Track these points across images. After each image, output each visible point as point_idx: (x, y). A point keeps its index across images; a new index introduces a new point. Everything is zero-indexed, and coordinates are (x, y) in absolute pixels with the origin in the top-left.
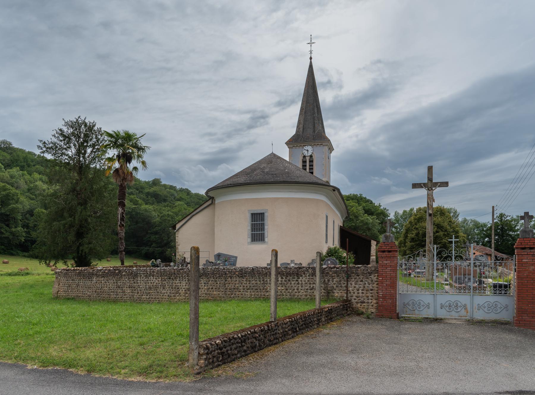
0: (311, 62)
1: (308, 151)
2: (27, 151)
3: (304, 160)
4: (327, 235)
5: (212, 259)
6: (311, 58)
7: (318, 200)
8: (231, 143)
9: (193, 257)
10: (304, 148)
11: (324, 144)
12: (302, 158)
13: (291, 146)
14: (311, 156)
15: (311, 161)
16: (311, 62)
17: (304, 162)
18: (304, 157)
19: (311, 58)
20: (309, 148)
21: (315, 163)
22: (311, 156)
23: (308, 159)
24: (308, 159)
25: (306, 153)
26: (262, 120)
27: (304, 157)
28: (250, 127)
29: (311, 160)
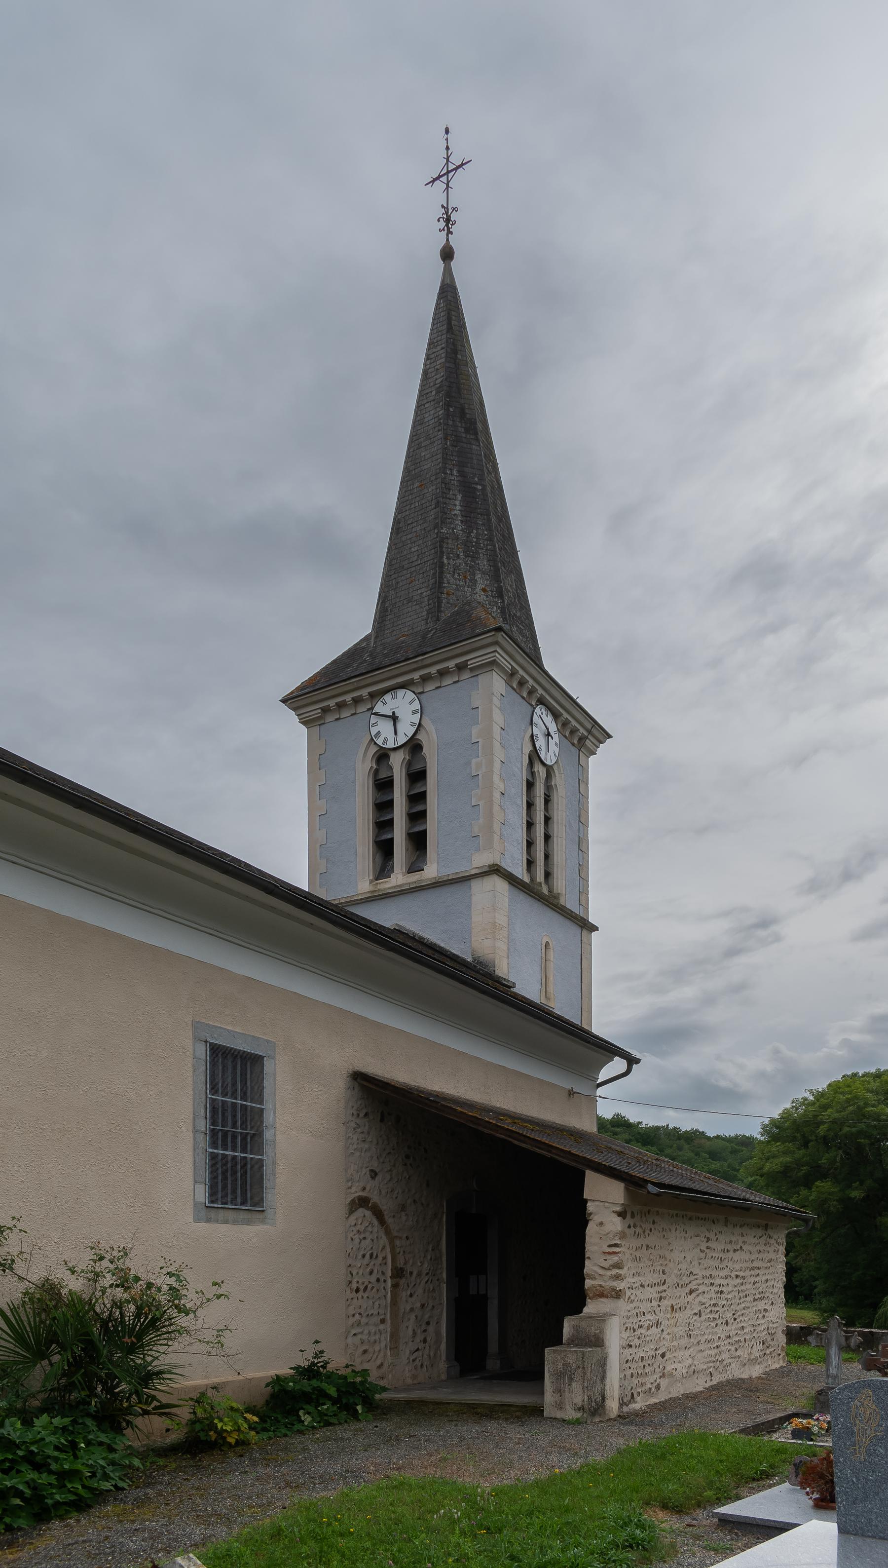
0: (448, 273)
1: (394, 718)
2: (683, 1130)
3: (383, 775)
5: (133, 1272)
6: (447, 254)
8: (685, 994)
10: (379, 708)
11: (473, 658)
13: (314, 711)
14: (414, 746)
16: (448, 273)
18: (383, 756)
19: (447, 254)
20: (403, 704)
21: (431, 785)
22: (414, 746)
24: (397, 761)
26: (761, 933)
27: (383, 756)
28: (732, 952)
29: (417, 767)
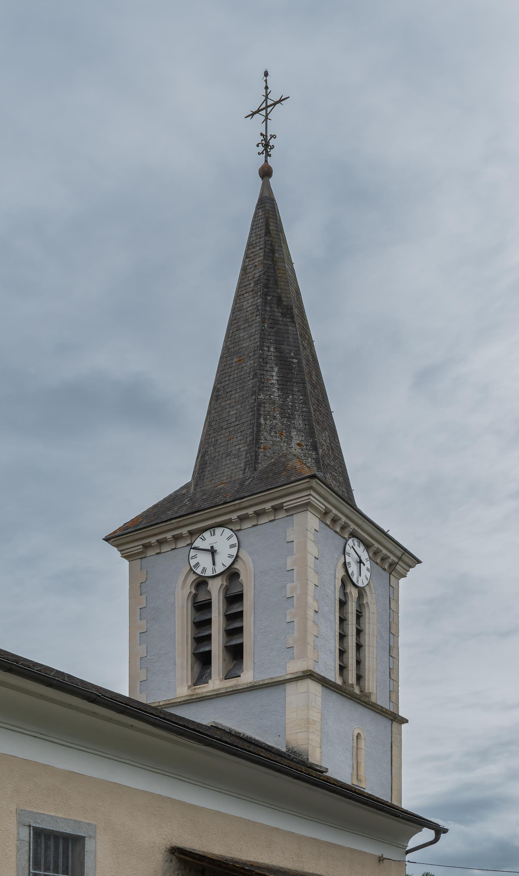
0: (266, 188)
1: (213, 552)
3: (202, 598)
4: (392, 755)
6: (266, 173)
7: (352, 851)
9: (314, 773)
10: (198, 543)
11: (289, 501)
12: (189, 589)
13: (136, 547)
14: (232, 574)
15: (234, 598)
16: (266, 188)
17: (202, 607)
18: (201, 583)
19: (266, 173)
20: (222, 541)
22: (232, 574)
23: (216, 590)
24: (216, 590)
25: (204, 564)
27: (201, 583)
29: (235, 591)
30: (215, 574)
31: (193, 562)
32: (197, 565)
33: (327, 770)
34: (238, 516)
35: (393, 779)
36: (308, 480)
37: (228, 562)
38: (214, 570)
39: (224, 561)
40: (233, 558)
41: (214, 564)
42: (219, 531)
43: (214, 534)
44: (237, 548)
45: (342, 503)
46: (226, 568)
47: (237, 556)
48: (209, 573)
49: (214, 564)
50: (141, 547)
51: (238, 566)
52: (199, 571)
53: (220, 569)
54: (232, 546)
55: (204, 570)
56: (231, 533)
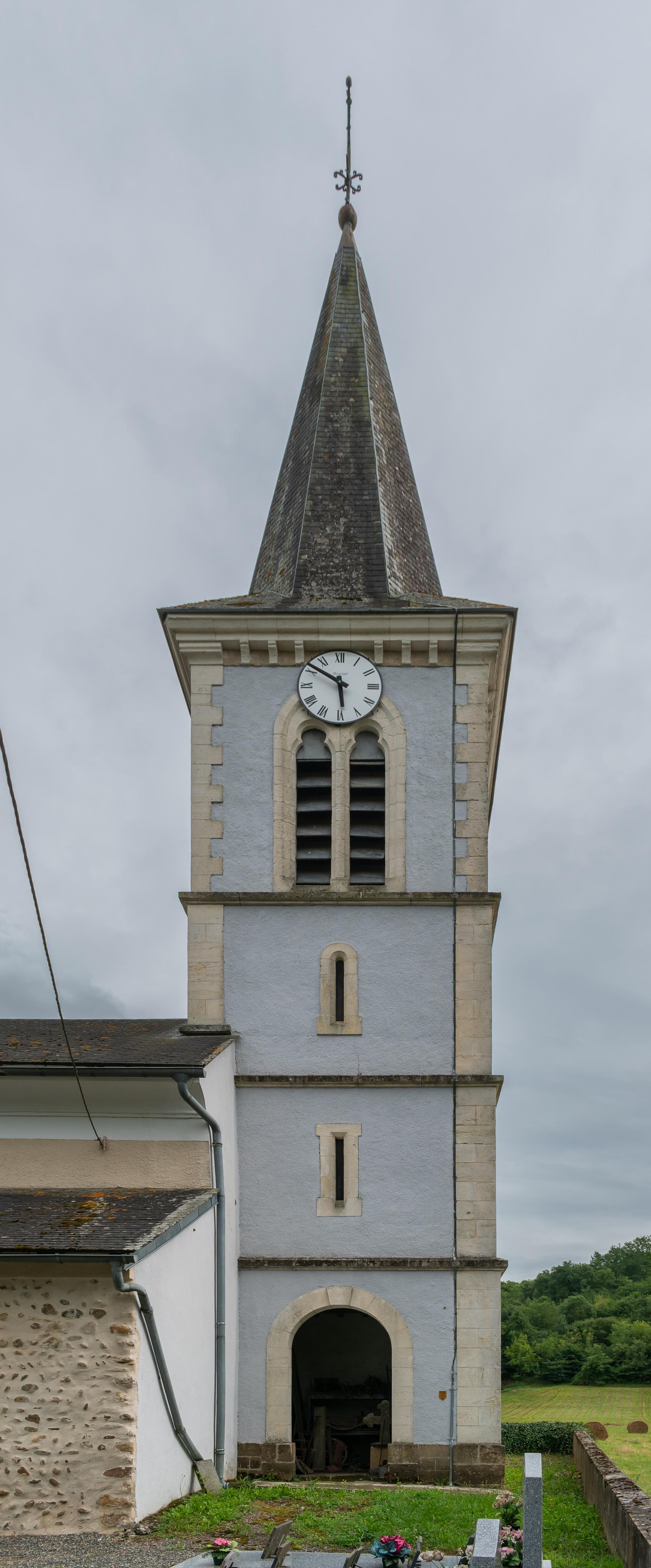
14: (366, 731)
17: (312, 770)
18: (315, 730)
22: (366, 731)
25: (324, 700)
27: (315, 730)
30: (341, 721)
31: (305, 694)
32: (312, 699)
33: (597, 1255)
34: (384, 642)
35: (458, 1002)
36: (504, 616)
37: (365, 710)
38: (340, 715)
39: (357, 705)
40: (373, 706)
41: (342, 704)
42: (350, 658)
43: (343, 661)
44: (380, 691)
45: (247, 619)
46: (360, 717)
47: (379, 705)
48: (331, 717)
49: (342, 704)
50: (219, 645)
51: (379, 718)
52: (314, 709)
53: (349, 716)
54: (371, 687)
55: (323, 710)
56: (373, 667)
